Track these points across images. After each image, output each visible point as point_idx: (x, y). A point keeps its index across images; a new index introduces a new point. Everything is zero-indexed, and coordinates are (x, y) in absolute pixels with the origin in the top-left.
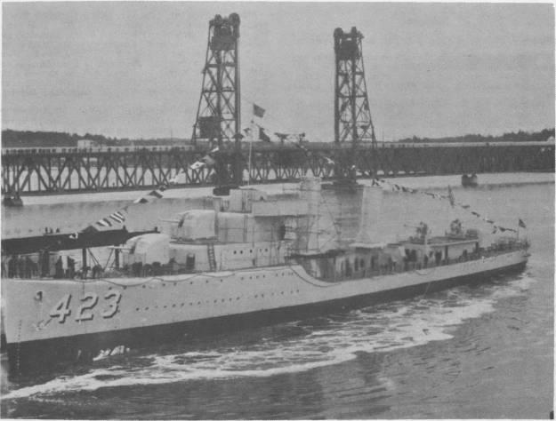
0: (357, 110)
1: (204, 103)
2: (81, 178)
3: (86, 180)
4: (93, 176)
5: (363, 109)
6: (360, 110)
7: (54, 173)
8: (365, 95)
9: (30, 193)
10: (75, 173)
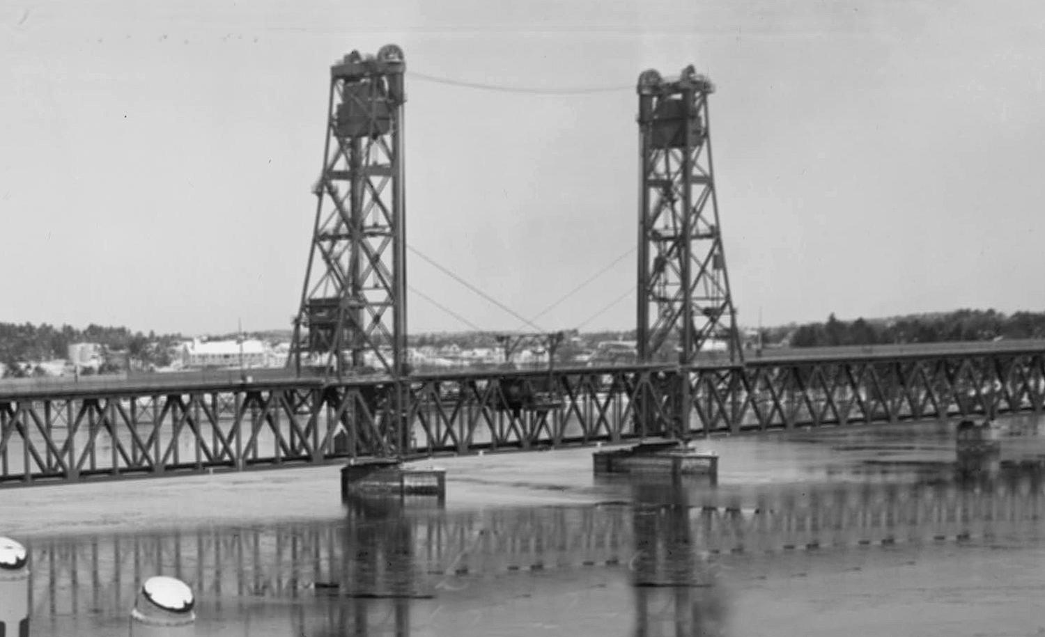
0: (695, 270)
1: (320, 266)
5: (709, 267)
10: (101, 438)
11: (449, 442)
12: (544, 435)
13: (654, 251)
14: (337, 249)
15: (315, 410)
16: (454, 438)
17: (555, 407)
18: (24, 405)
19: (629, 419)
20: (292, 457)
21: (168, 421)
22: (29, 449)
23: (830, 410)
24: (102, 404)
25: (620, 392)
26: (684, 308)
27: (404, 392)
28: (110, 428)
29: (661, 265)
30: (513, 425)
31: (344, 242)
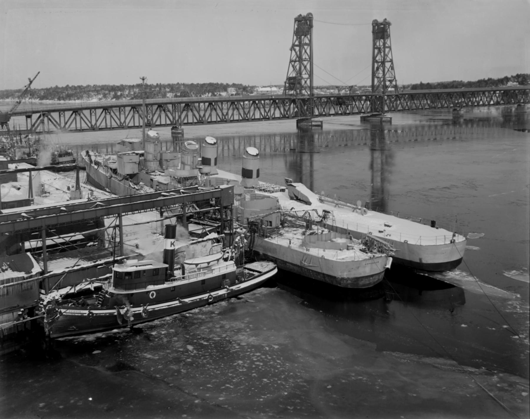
0: (386, 70)
1: (291, 69)
5: (390, 69)
6: (388, 70)
8: (391, 61)
12: (348, 112)
13: (376, 65)
15: (290, 105)
18: (216, 103)
19: (370, 108)
20: (284, 117)
22: (217, 114)
23: (420, 106)
24: (236, 103)
29: (378, 69)
30: (340, 109)
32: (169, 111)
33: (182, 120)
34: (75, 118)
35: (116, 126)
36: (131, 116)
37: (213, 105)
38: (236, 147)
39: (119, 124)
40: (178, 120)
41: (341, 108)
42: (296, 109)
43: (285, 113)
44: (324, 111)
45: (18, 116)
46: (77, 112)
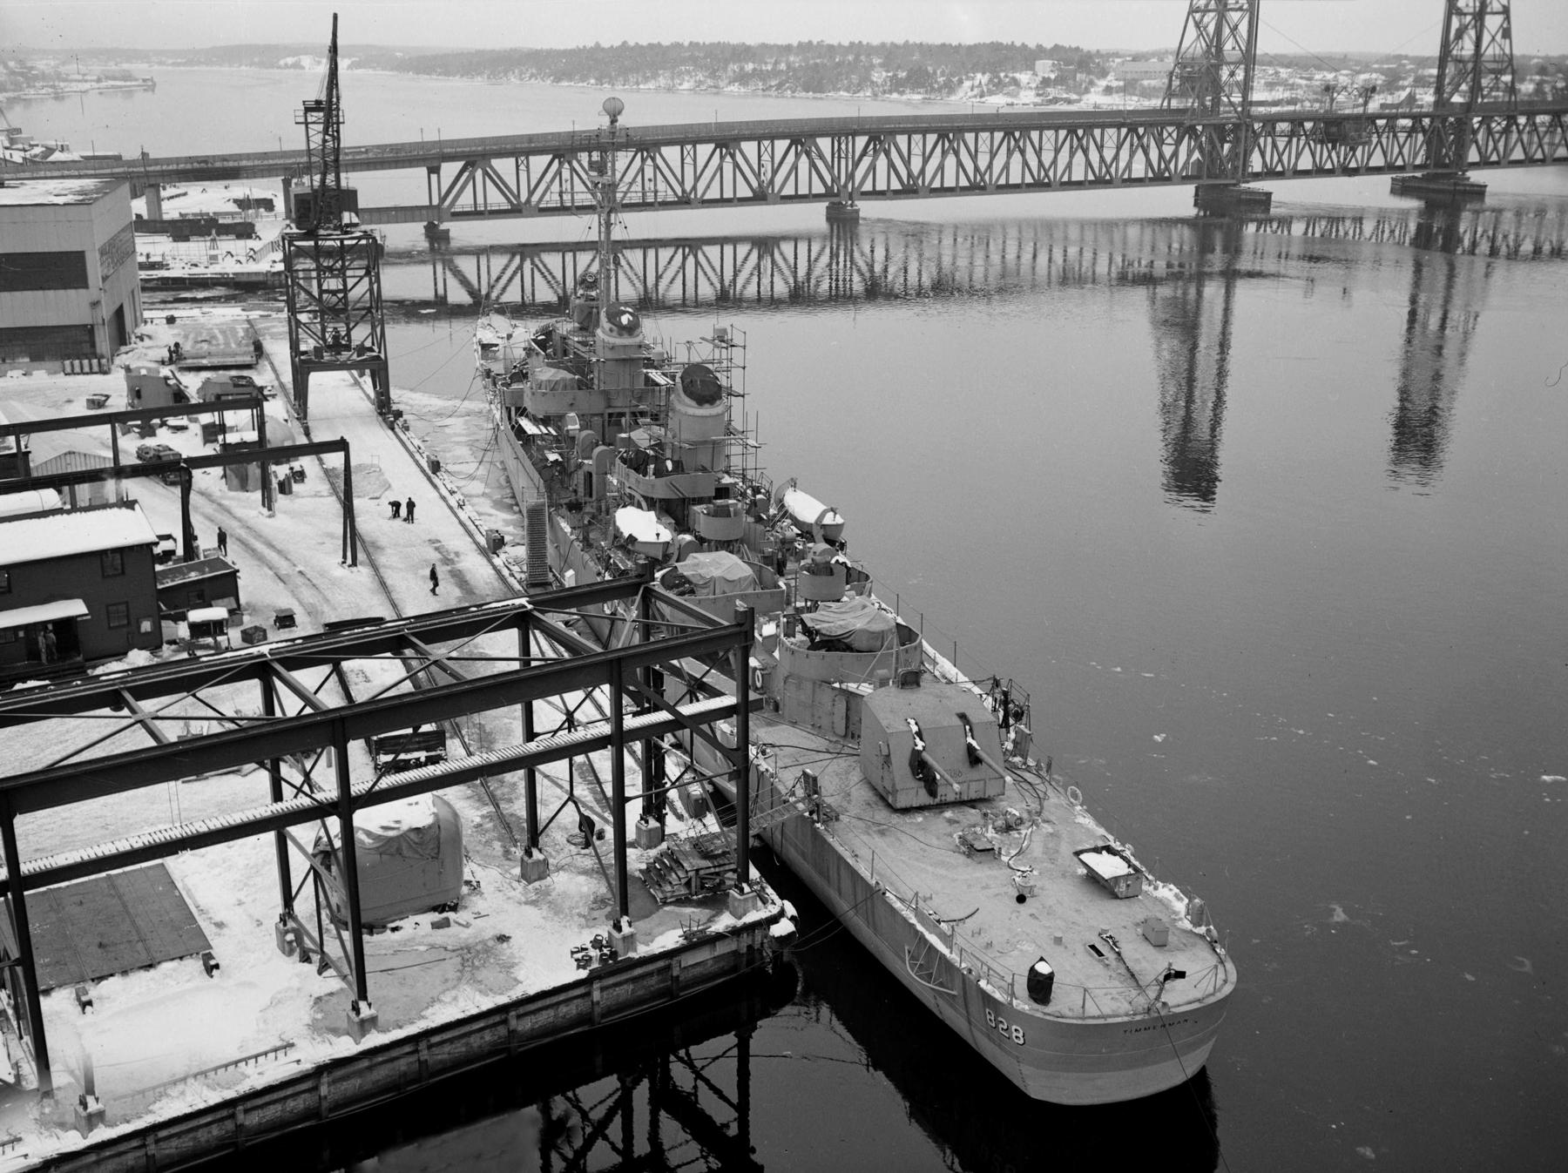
0: (1486, 38)
1: (1192, 32)
2: (1089, 164)
3: (1096, 166)
4: (1168, 156)
5: (1498, 38)
6: (1493, 39)
7: (1168, 151)
8: (1506, 11)
9: (875, 194)
10: (1017, 157)
11: (1279, 168)
12: (1353, 165)
13: (1455, 23)
14: (1206, 20)
15: (1178, 142)
16: (1283, 166)
17: (1364, 144)
18: (958, 135)
19: (1422, 152)
20: (1159, 178)
21: (1127, 145)
22: (1026, 164)
23: (1540, 151)
24: (1017, 134)
25: (1417, 132)
26: (1474, 69)
27: (1247, 131)
28: (1086, 152)
29: (1460, 34)
30: (1330, 156)
31: (1212, 14)
32: (821, 156)
33: (856, 185)
34: (559, 173)
35: (671, 198)
36: (731, 166)
37: (949, 141)
38: (1011, 256)
39: (680, 193)
40: (845, 186)
41: (1334, 154)
42: (1196, 155)
43: (1163, 166)
44: (1280, 160)
45: (390, 168)
46: (563, 156)
